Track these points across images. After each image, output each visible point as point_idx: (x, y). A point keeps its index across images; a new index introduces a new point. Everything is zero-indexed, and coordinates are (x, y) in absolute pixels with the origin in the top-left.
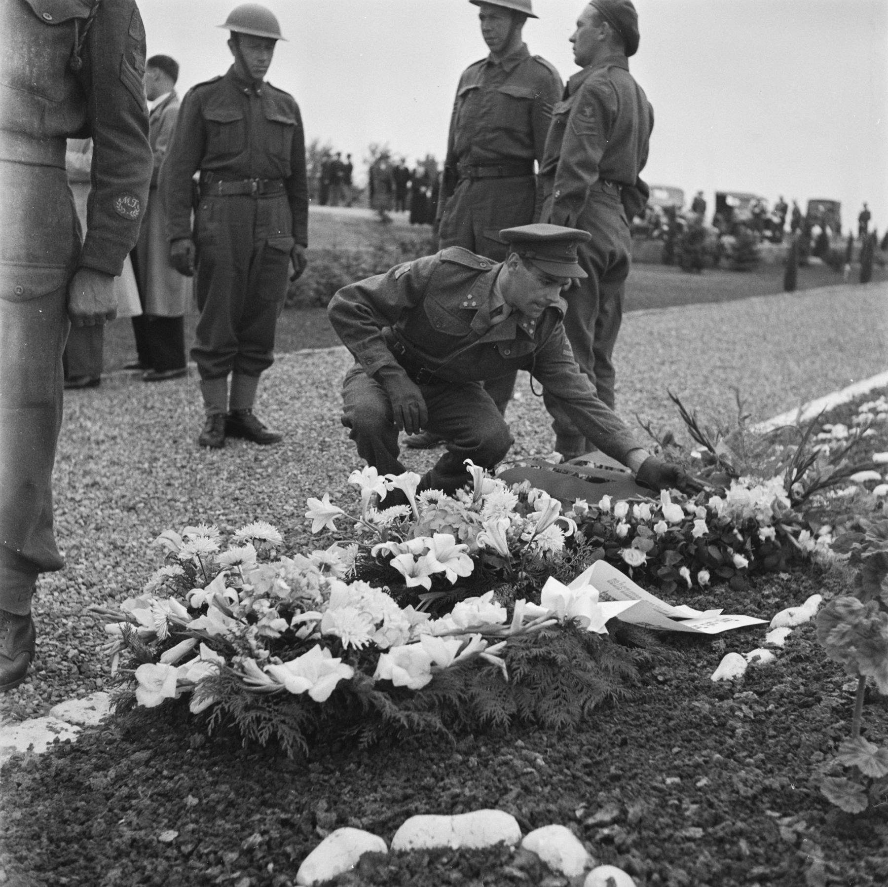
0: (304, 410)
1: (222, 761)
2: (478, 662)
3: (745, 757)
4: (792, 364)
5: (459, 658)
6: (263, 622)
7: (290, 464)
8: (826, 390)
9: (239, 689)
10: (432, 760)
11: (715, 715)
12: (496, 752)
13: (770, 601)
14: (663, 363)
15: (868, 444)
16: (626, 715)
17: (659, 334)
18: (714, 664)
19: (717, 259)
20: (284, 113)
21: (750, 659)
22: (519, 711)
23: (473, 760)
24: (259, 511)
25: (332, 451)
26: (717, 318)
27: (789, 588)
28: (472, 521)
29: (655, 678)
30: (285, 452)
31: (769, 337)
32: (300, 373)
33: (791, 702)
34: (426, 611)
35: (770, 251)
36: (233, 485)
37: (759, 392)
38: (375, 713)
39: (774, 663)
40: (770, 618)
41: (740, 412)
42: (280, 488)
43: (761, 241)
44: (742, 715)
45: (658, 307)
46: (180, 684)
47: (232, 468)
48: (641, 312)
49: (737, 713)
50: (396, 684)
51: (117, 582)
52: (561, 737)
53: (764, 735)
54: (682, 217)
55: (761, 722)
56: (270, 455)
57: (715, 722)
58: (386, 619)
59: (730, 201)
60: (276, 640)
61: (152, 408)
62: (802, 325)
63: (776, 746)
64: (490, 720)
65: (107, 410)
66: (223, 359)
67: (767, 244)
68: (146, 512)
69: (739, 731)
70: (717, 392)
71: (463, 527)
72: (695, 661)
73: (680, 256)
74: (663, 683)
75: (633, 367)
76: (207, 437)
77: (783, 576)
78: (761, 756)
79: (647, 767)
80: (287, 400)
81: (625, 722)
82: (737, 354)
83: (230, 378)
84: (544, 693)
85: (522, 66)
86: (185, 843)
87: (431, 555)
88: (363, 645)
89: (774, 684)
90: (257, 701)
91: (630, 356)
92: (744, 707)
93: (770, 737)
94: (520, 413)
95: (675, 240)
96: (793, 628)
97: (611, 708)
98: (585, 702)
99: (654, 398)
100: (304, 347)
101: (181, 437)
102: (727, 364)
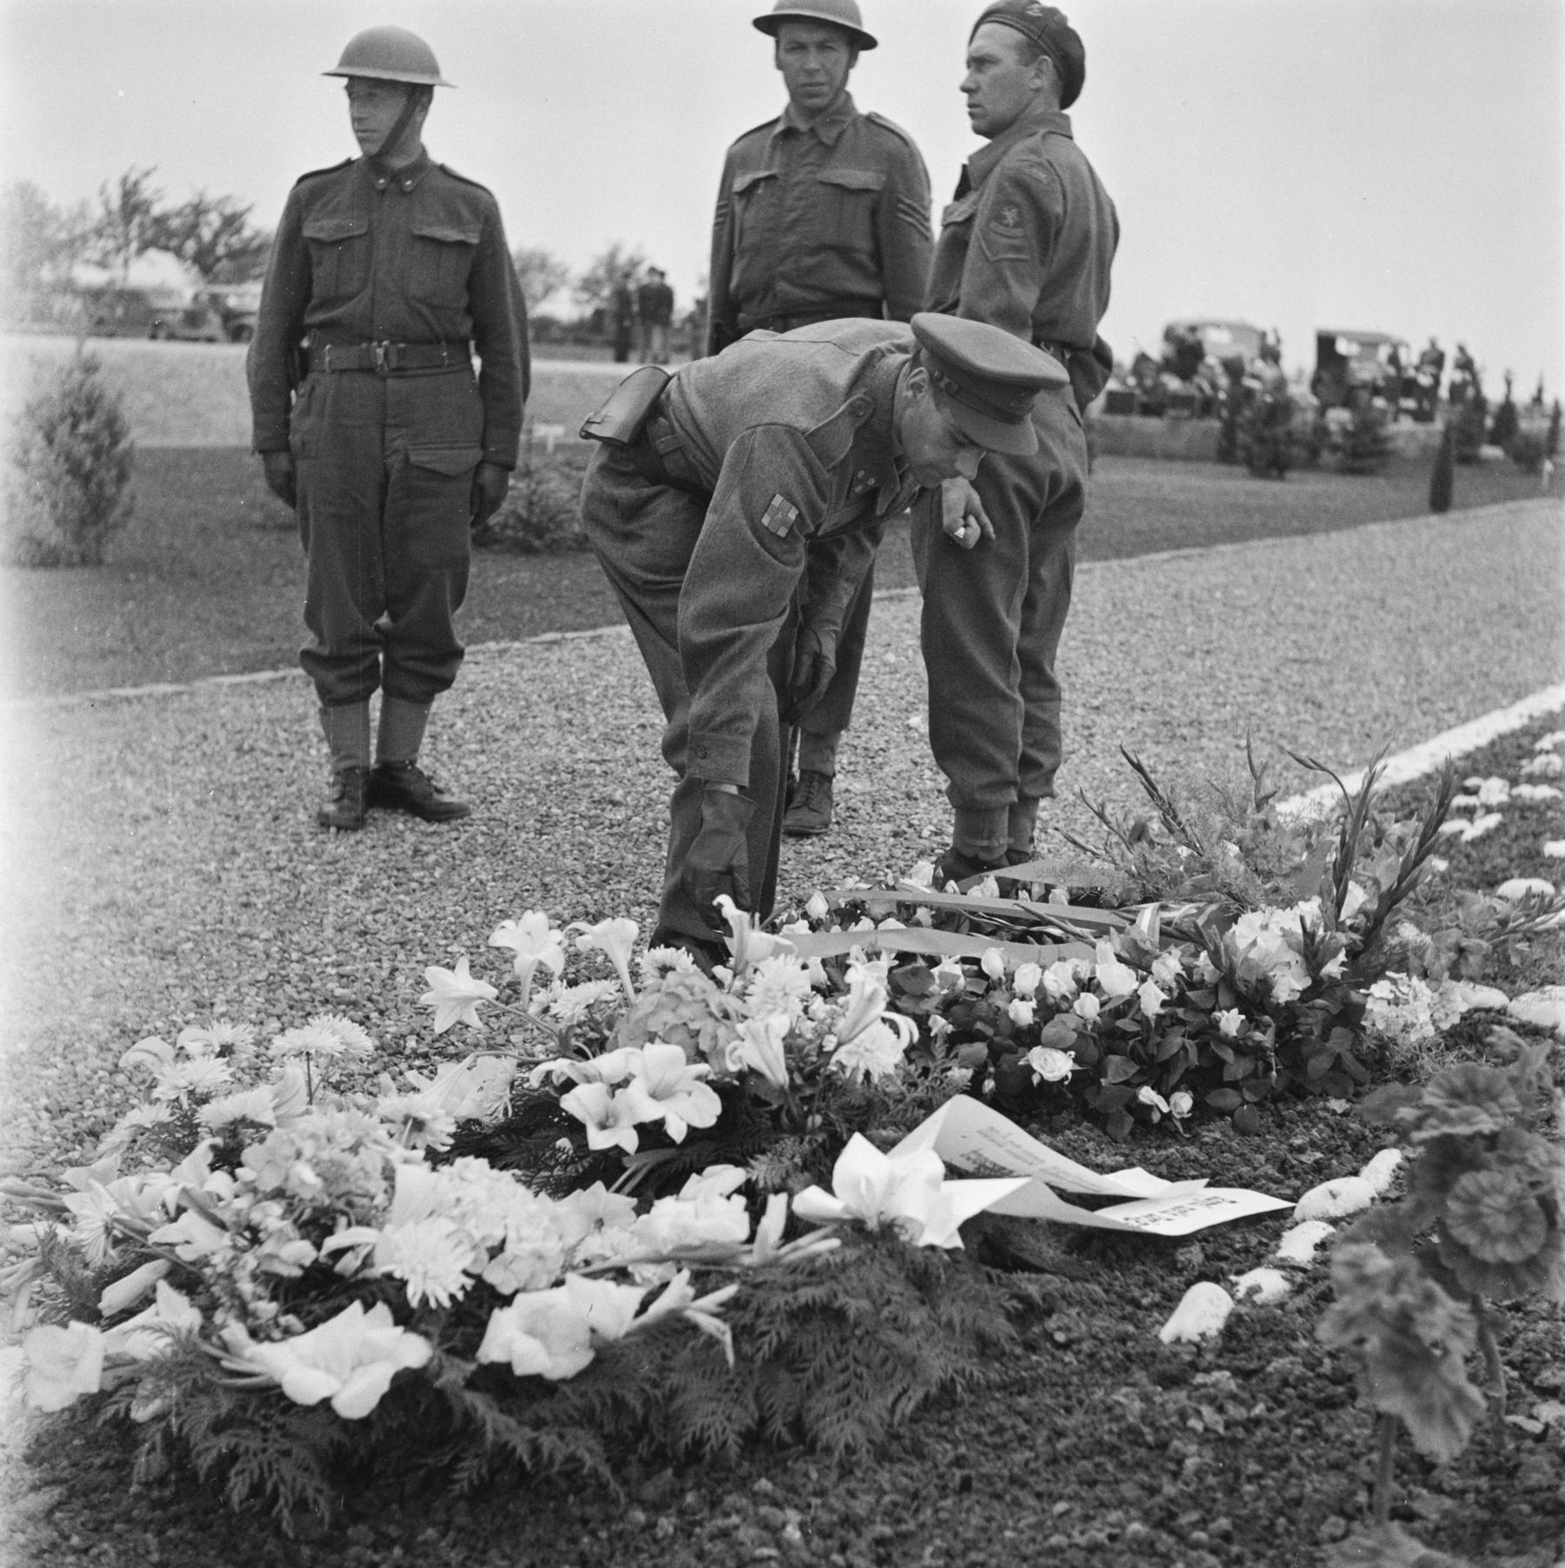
0: (525, 752)
1: (192, 1512)
2: (677, 1327)
3: (1194, 1525)
4: (1426, 653)
5: (644, 1319)
6: (268, 1247)
7: (479, 860)
8: (1483, 705)
9: (210, 1384)
10: (585, 1521)
11: (1152, 1425)
12: (714, 1504)
13: (1303, 1158)
14: (1191, 655)
15: (1541, 820)
16: (982, 1420)
17: (1192, 597)
18: (1169, 1303)
19: (1314, 453)
20: (455, 219)
21: (1241, 1292)
22: (763, 1422)
23: (666, 1525)
24: (401, 956)
25: (559, 833)
26: (1301, 566)
27: (1343, 1131)
28: (727, 1016)
29: (1049, 1336)
30: (473, 837)
31: (1390, 601)
32: (532, 680)
33: (1303, 1397)
34: (630, 1194)
35: (1412, 435)
36: (364, 905)
37: (1360, 710)
39: (1282, 1306)
40: (1295, 1197)
41: (1258, 789)
42: (450, 909)
43: (1396, 420)
44: (1199, 1427)
45: (1197, 545)
46: (112, 1363)
47: (368, 870)
48: (1165, 555)
49: (1193, 1423)
50: (519, 1370)
51: (109, 1105)
52: (846, 1471)
53: (1237, 1473)
54: (1255, 377)
55: (1235, 1442)
56: (444, 840)
57: (1150, 1438)
58: (512, 1236)
59: (1342, 347)
60: (291, 1280)
61: (252, 749)
62: (1455, 577)
63: (1257, 1498)
65: (169, 755)
66: (353, 669)
67: (1406, 424)
68: (194, 958)
69: (1191, 1463)
70: (1282, 709)
71: (707, 1026)
72: (1137, 1293)
73: (1246, 448)
74: (1065, 1346)
75: (1136, 662)
76: (330, 808)
77: (1338, 1105)
78: (1224, 1523)
79: (997, 1548)
80: (497, 732)
81: (978, 1437)
82: (1328, 636)
83: (376, 699)
84: (820, 1380)
85: (849, 134)
87: (637, 1091)
88: (452, 1297)
89: (1276, 1353)
90: (244, 1408)
91: (1134, 640)
92: (1206, 1410)
93: (1250, 1479)
94: (915, 755)
95: (1240, 419)
96: (1334, 1221)
97: (955, 1404)
98: (895, 1403)
99: (1165, 724)
100: (550, 629)
101: (288, 809)
102: (1307, 655)
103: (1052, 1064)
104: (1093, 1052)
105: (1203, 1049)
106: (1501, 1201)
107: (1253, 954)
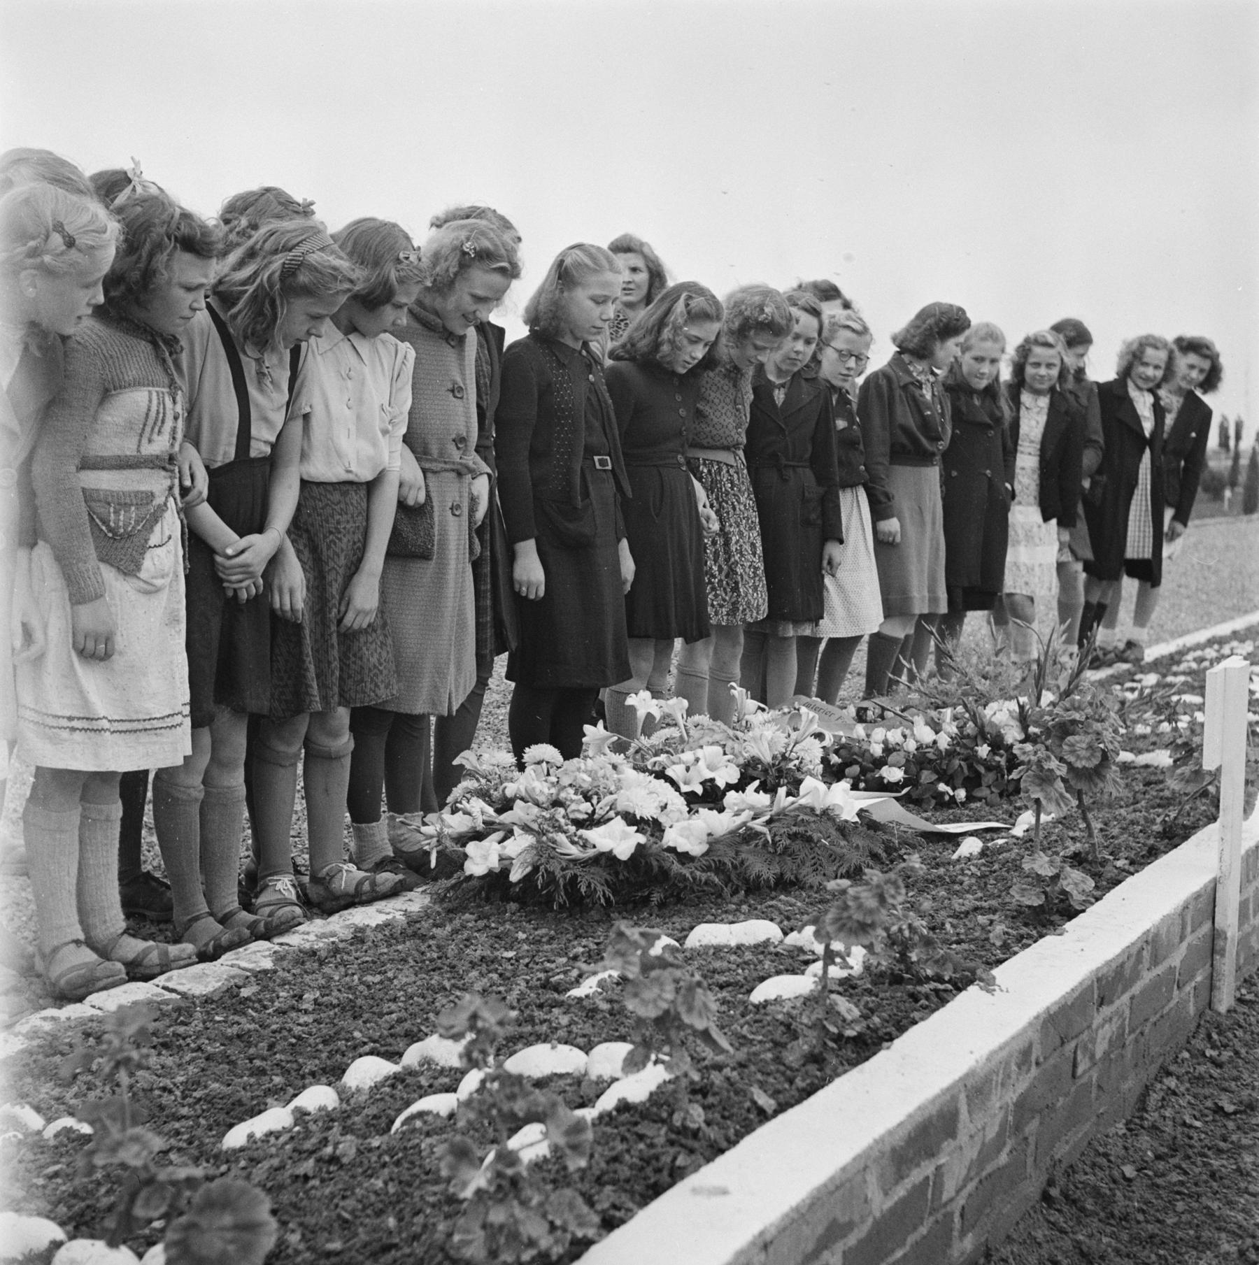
38: (664, 873)
49: (967, 872)
64: (758, 877)
69: (966, 883)
84: (803, 863)
86: (523, 957)
103: (893, 774)
104: (914, 769)
105: (970, 767)
106: (1084, 746)
107: (993, 719)
